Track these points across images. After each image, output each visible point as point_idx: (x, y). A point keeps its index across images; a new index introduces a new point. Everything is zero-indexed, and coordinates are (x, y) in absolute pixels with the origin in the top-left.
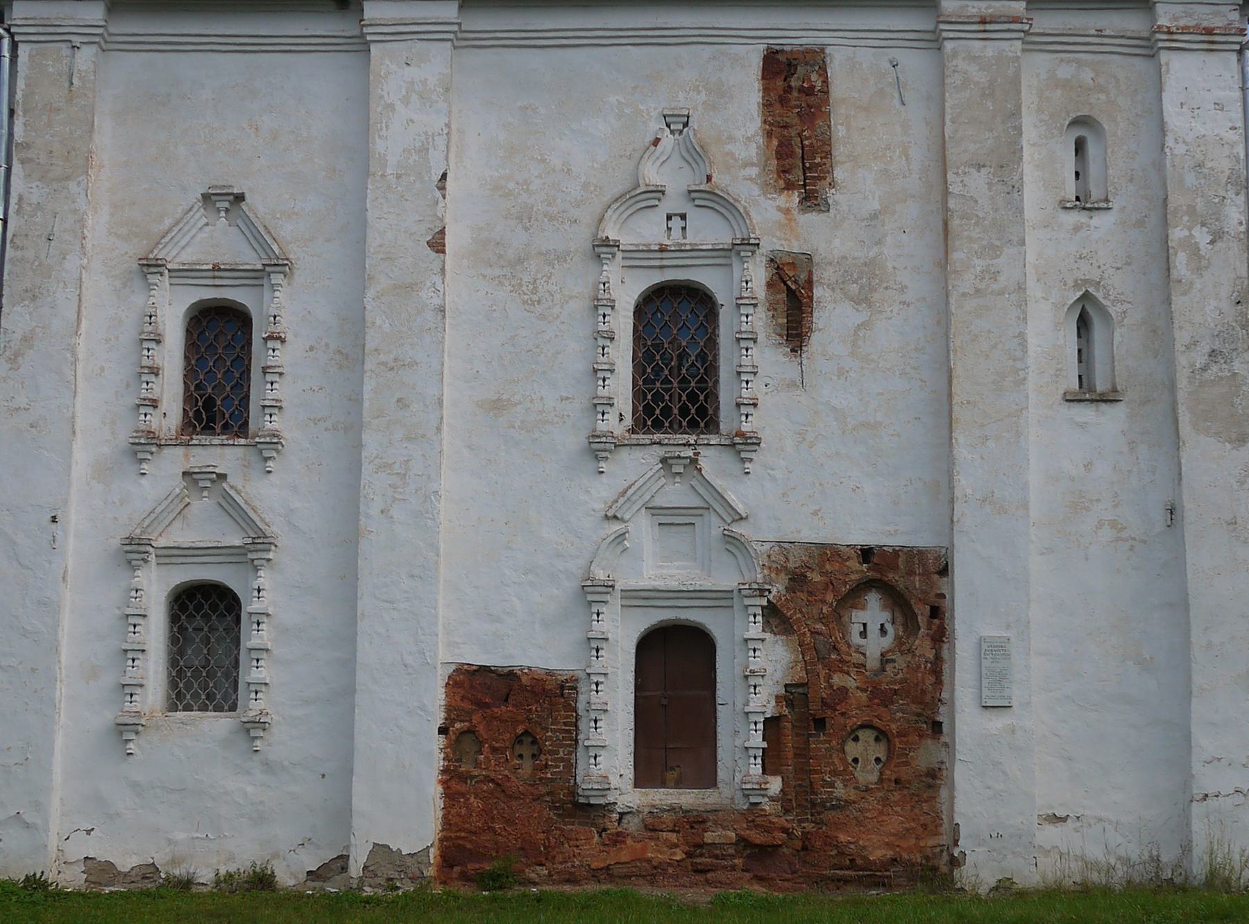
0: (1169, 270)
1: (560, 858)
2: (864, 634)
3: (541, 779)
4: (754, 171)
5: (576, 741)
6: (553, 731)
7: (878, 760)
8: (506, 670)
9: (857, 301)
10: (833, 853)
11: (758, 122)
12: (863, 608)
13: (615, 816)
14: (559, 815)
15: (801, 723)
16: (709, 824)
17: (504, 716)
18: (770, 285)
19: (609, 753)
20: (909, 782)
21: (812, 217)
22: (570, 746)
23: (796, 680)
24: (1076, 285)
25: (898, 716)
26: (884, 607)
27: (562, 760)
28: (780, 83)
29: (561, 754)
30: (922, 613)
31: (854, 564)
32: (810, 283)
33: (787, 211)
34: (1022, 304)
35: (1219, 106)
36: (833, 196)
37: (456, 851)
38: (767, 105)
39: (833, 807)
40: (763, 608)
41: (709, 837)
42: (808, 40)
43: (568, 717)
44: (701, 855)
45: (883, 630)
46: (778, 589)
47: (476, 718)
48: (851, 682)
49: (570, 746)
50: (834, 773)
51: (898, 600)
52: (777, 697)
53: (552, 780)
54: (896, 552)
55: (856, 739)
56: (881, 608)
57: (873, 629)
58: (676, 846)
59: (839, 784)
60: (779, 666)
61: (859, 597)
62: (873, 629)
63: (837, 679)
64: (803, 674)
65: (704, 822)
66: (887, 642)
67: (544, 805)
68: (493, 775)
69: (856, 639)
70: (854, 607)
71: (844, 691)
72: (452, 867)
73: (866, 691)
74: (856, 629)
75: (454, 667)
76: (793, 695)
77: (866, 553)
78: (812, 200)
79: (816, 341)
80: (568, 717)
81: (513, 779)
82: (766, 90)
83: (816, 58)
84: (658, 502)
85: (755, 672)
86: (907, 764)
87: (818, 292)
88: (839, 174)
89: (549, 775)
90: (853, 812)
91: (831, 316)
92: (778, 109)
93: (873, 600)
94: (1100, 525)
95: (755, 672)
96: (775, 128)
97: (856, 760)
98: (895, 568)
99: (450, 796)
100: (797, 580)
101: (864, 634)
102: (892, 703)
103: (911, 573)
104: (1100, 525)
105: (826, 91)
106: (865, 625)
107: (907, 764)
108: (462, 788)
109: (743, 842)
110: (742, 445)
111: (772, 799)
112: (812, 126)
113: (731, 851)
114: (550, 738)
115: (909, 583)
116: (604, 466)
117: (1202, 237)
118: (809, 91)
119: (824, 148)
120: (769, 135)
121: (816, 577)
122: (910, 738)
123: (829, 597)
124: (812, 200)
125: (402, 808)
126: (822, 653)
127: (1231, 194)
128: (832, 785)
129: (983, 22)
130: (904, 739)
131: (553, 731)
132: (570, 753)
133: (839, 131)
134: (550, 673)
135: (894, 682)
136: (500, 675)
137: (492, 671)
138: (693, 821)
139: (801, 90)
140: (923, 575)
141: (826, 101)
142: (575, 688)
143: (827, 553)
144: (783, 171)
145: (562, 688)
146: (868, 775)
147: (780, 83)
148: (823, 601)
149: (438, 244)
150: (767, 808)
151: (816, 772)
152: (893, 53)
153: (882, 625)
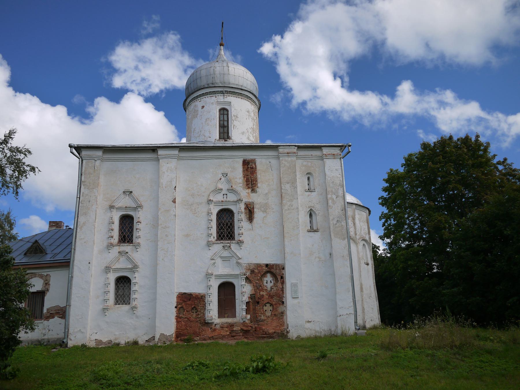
2: (267, 283)
9: (263, 212)
15: (254, 302)
17: (189, 304)
18: (245, 209)
19: (212, 311)
21: (254, 194)
24: (309, 207)
25: (274, 301)
28: (246, 166)
30: (279, 278)
31: (264, 268)
32: (253, 208)
33: (248, 193)
34: (298, 211)
36: (258, 190)
37: (178, 335)
41: (235, 329)
42: (252, 157)
46: (248, 274)
48: (264, 293)
50: (261, 313)
51: (274, 275)
54: (273, 265)
57: (269, 282)
62: (269, 282)
63: (261, 293)
66: (272, 284)
69: (265, 284)
71: (263, 295)
74: (265, 282)
77: (267, 265)
79: (255, 220)
83: (253, 161)
84: (222, 256)
85: (244, 292)
87: (255, 210)
88: (259, 185)
90: (265, 322)
91: (258, 215)
92: (246, 172)
93: (269, 275)
94: (316, 258)
95: (244, 292)
96: (245, 176)
99: (178, 322)
100: (252, 272)
101: (267, 283)
103: (276, 269)
108: (180, 320)
112: (253, 175)
115: (276, 271)
117: (334, 197)
118: (252, 168)
121: (256, 271)
123: (259, 275)
124: (253, 191)
125: (167, 325)
126: (258, 287)
129: (288, 153)
133: (259, 176)
134: (199, 294)
138: (231, 325)
139: (251, 168)
143: (259, 266)
144: (247, 185)
146: (269, 314)
147: (246, 166)
149: (174, 201)
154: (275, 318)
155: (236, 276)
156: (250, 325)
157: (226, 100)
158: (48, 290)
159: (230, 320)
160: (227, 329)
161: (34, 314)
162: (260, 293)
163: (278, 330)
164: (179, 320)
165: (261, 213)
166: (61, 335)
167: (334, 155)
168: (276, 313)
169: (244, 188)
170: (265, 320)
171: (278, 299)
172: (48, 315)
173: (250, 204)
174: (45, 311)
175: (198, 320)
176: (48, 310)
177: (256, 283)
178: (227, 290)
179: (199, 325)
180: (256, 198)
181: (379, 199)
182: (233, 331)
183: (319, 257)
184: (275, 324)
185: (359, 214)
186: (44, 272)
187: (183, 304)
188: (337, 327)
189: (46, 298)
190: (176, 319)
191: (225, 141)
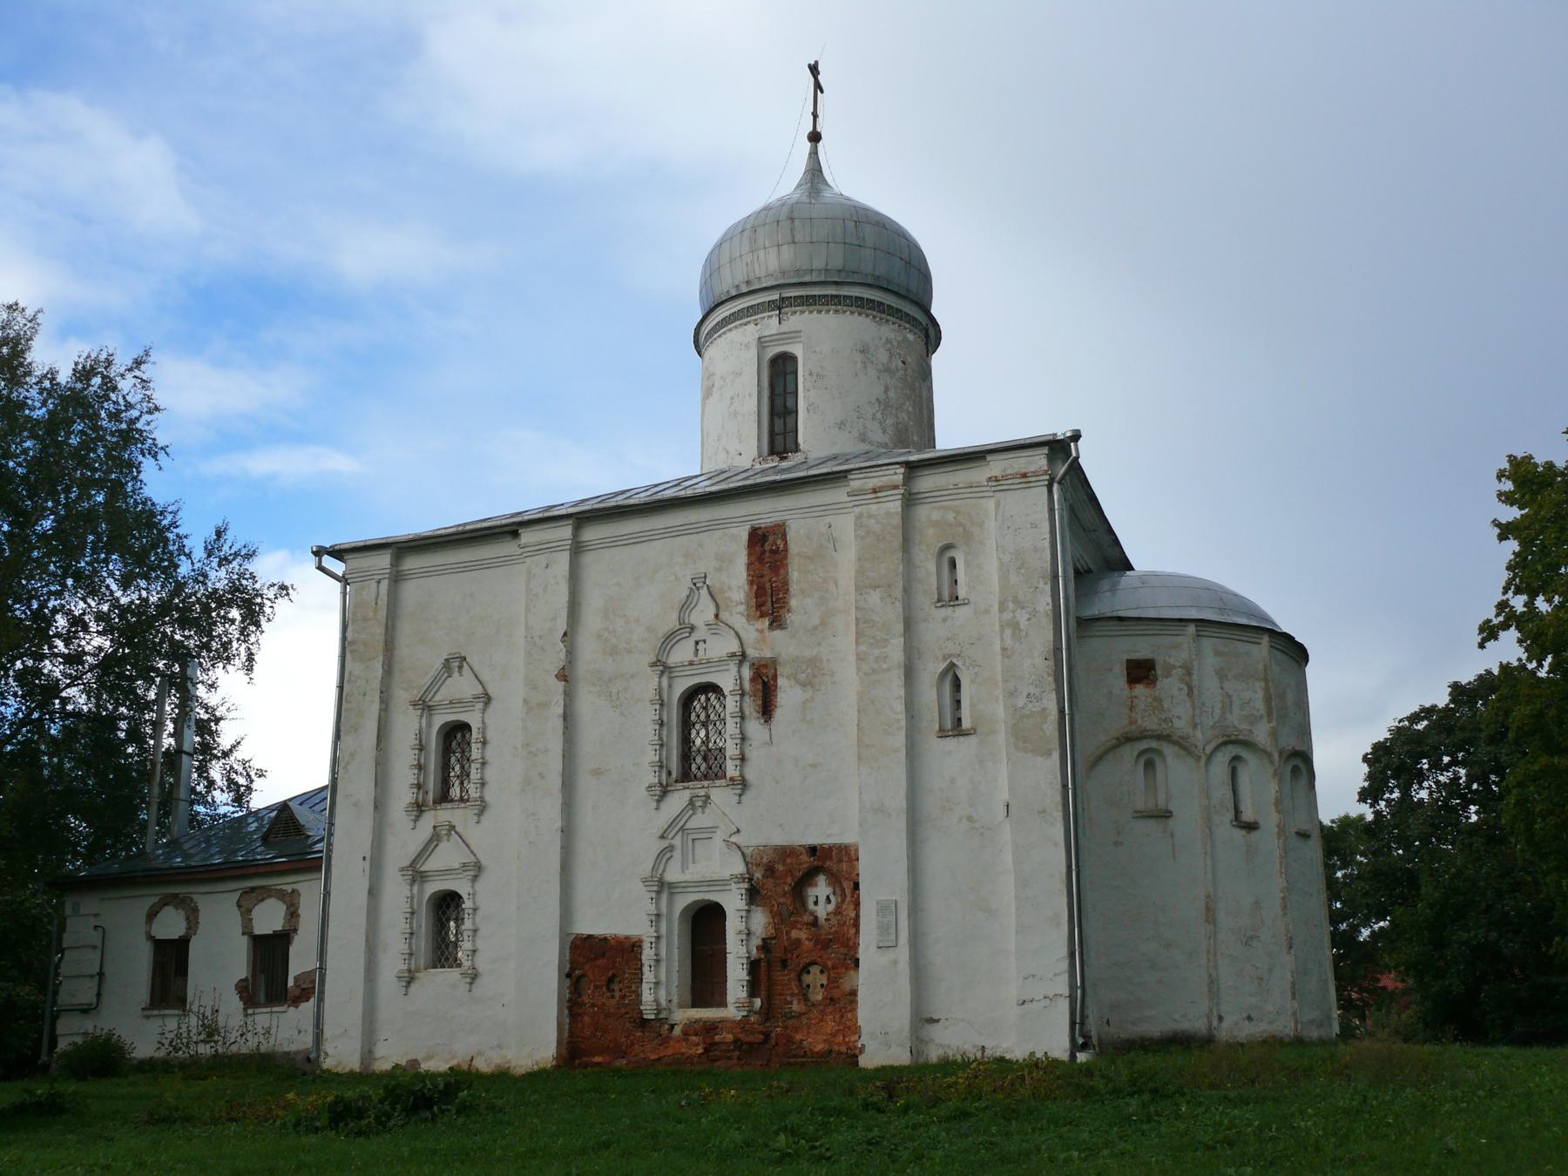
0: (1120, 619)
4: (742, 608)
9: (803, 685)
11: (744, 575)
17: (597, 966)
18: (752, 680)
19: (660, 986)
21: (778, 633)
24: (945, 659)
25: (835, 953)
26: (829, 884)
28: (758, 549)
30: (848, 886)
31: (805, 858)
32: (775, 677)
33: (762, 631)
35: (1034, 526)
37: (573, 1051)
38: (750, 565)
42: (775, 518)
45: (828, 900)
48: (801, 934)
50: (792, 995)
51: (835, 880)
54: (831, 848)
56: (798, 876)
57: (822, 899)
62: (822, 899)
63: (794, 934)
66: (831, 907)
69: (811, 906)
71: (798, 941)
74: (811, 900)
76: (765, 946)
77: (813, 850)
78: (777, 622)
79: (779, 714)
82: (750, 555)
83: (780, 530)
87: (780, 681)
88: (793, 603)
91: (788, 695)
92: (757, 565)
93: (822, 880)
94: (960, 821)
98: (831, 858)
100: (770, 870)
101: (816, 903)
103: (840, 861)
104: (960, 821)
105: (786, 550)
109: (736, 1040)
112: (777, 575)
115: (830, 862)
118: (775, 552)
119: (784, 587)
120: (751, 583)
121: (781, 868)
123: (789, 880)
124: (777, 622)
126: (781, 919)
127: (1041, 585)
129: (875, 491)
134: (627, 938)
138: (710, 1028)
139: (771, 551)
141: (786, 557)
143: (786, 852)
144: (759, 606)
146: (818, 996)
147: (758, 549)
152: (828, 519)
154: (830, 1009)
157: (786, 327)
158: (295, 930)
161: (1082, 1024)
163: (839, 1044)
165: (798, 690)
166: (306, 1041)
167: (1024, 475)
168: (836, 993)
169: (749, 618)
170: (801, 1014)
171: (839, 948)
172: (297, 992)
173: (765, 666)
174: (291, 983)
176: (296, 979)
180: (778, 645)
183: (970, 819)
184: (830, 1025)
185: (1217, 653)
186: (286, 883)
187: (587, 967)
189: (293, 950)
191: (783, 459)
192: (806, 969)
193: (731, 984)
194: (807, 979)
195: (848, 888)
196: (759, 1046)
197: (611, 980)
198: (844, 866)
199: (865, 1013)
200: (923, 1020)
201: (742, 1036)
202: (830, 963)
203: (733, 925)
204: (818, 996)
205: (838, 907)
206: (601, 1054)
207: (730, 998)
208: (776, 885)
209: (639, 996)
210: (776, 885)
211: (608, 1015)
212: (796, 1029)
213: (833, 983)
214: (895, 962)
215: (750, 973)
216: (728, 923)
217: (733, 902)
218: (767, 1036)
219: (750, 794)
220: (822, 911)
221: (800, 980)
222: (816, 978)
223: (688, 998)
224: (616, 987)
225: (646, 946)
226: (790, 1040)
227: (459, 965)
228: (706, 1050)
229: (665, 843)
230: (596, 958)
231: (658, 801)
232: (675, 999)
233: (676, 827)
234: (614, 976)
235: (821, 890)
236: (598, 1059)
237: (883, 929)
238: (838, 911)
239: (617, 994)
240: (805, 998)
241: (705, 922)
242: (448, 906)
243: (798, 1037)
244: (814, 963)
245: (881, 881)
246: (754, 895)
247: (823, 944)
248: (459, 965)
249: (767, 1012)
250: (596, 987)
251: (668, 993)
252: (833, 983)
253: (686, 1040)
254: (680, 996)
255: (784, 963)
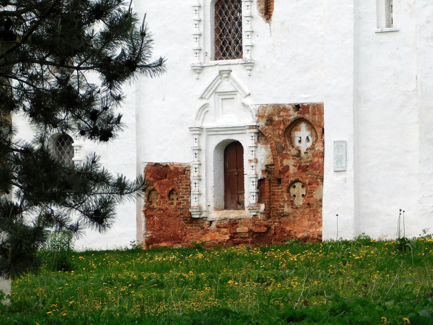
1: (186, 240)
2: (300, 141)
3: (179, 208)
5: (190, 192)
6: (182, 188)
7: (303, 195)
8: (165, 164)
10: (286, 235)
12: (300, 130)
13: (207, 223)
14: (186, 223)
15: (272, 181)
16: (239, 224)
19: (205, 196)
20: (313, 204)
22: (188, 194)
23: (270, 163)
26: (308, 129)
27: (185, 200)
29: (185, 198)
31: (292, 112)
39: (284, 216)
40: (255, 133)
41: (238, 230)
43: (187, 182)
44: (237, 237)
46: (262, 123)
47: (155, 184)
49: (188, 194)
50: (284, 202)
51: (311, 126)
52: (262, 171)
53: (182, 209)
55: (294, 187)
56: (291, 125)
57: (304, 139)
58: (226, 234)
59: (286, 206)
60: (263, 157)
61: (298, 125)
62: (304, 139)
63: (285, 162)
64: (272, 160)
65: (236, 224)
66: (309, 144)
67: (181, 219)
68: (161, 207)
69: (297, 144)
70: (296, 130)
72: (149, 245)
73: (296, 166)
75: (146, 164)
76: (268, 170)
77: (297, 107)
80: (187, 182)
81: (169, 209)
84: (219, 90)
85: (255, 160)
86: (312, 197)
89: (181, 207)
90: (291, 218)
93: (303, 126)
95: (255, 160)
97: (294, 196)
98: (308, 112)
99: (148, 217)
100: (270, 121)
101: (300, 141)
102: (306, 171)
103: (314, 114)
106: (301, 137)
107: (211, 222)
108: (151, 213)
109: (250, 231)
110: (250, 65)
111: (261, 213)
113: (247, 235)
114: (181, 192)
115: (308, 116)
116: (152, 60)
121: (276, 118)
122: (313, 185)
126: (279, 152)
128: (283, 207)
130: (311, 186)
131: (182, 188)
132: (188, 197)
134: (180, 165)
135: (307, 162)
136: (163, 166)
137: (161, 165)
138: (234, 223)
140: (319, 114)
142: (189, 170)
143: (279, 109)
145: (185, 171)
146: (299, 202)
148: (279, 129)
150: (259, 217)
151: (277, 201)
153: (307, 137)
154: (307, 211)
155: (241, 129)
156: (266, 223)
159: (233, 214)
160: (225, 230)
162: (281, 161)
164: (149, 213)
168: (311, 201)
171: (312, 171)
175: (179, 213)
177: (276, 142)
178: (231, 152)
179: (183, 222)
181: (161, 62)
182: (236, 233)
188: (81, 229)
190: (145, 212)
192: (292, 184)
193: (246, 195)
194: (293, 191)
195: (317, 129)
196: (263, 236)
197: (171, 193)
198: (317, 118)
199: (327, 213)
200: (358, 214)
201: (253, 228)
202: (307, 181)
203: (247, 156)
204: (299, 202)
205: (313, 145)
206: (166, 241)
207: (246, 204)
208: (274, 130)
209: (189, 203)
210: (274, 130)
211: (169, 216)
212: (287, 224)
213: (309, 194)
214: (345, 181)
215: (258, 187)
216: (245, 155)
217: (247, 141)
218: (269, 228)
219: (256, 69)
220: (304, 146)
221: (288, 191)
222: (298, 190)
223: (222, 204)
224: (174, 197)
225: (193, 170)
226: (283, 230)
227: (102, 86)
228: (232, 238)
229: (204, 102)
230: (161, 179)
231: (246, 96)
232: (212, 205)
233: (212, 90)
234: (173, 190)
235: (302, 133)
236: (164, 244)
237: (338, 159)
238: (312, 148)
239: (175, 202)
240: (292, 203)
241: (231, 152)
242: (63, 144)
243: (288, 229)
244: (297, 181)
245: (336, 128)
246: (260, 135)
247: (303, 169)
248: (102, 86)
249: (268, 214)
250: (162, 197)
251: (207, 200)
252: (309, 194)
253: (218, 231)
254: (216, 203)
255: (279, 180)
